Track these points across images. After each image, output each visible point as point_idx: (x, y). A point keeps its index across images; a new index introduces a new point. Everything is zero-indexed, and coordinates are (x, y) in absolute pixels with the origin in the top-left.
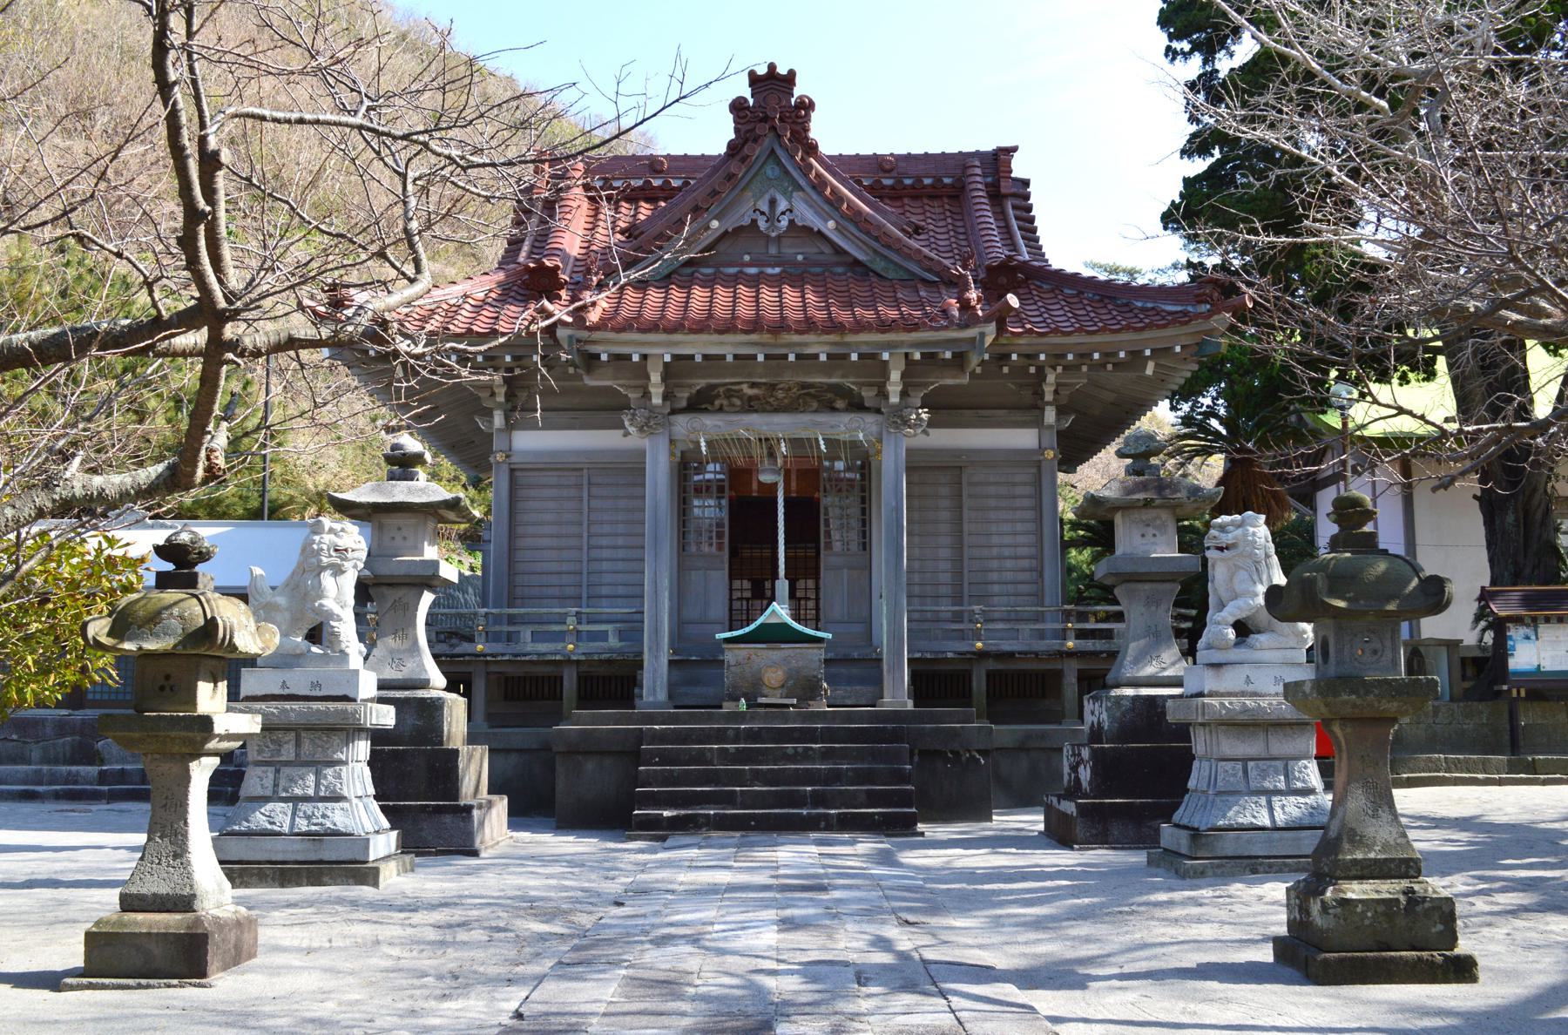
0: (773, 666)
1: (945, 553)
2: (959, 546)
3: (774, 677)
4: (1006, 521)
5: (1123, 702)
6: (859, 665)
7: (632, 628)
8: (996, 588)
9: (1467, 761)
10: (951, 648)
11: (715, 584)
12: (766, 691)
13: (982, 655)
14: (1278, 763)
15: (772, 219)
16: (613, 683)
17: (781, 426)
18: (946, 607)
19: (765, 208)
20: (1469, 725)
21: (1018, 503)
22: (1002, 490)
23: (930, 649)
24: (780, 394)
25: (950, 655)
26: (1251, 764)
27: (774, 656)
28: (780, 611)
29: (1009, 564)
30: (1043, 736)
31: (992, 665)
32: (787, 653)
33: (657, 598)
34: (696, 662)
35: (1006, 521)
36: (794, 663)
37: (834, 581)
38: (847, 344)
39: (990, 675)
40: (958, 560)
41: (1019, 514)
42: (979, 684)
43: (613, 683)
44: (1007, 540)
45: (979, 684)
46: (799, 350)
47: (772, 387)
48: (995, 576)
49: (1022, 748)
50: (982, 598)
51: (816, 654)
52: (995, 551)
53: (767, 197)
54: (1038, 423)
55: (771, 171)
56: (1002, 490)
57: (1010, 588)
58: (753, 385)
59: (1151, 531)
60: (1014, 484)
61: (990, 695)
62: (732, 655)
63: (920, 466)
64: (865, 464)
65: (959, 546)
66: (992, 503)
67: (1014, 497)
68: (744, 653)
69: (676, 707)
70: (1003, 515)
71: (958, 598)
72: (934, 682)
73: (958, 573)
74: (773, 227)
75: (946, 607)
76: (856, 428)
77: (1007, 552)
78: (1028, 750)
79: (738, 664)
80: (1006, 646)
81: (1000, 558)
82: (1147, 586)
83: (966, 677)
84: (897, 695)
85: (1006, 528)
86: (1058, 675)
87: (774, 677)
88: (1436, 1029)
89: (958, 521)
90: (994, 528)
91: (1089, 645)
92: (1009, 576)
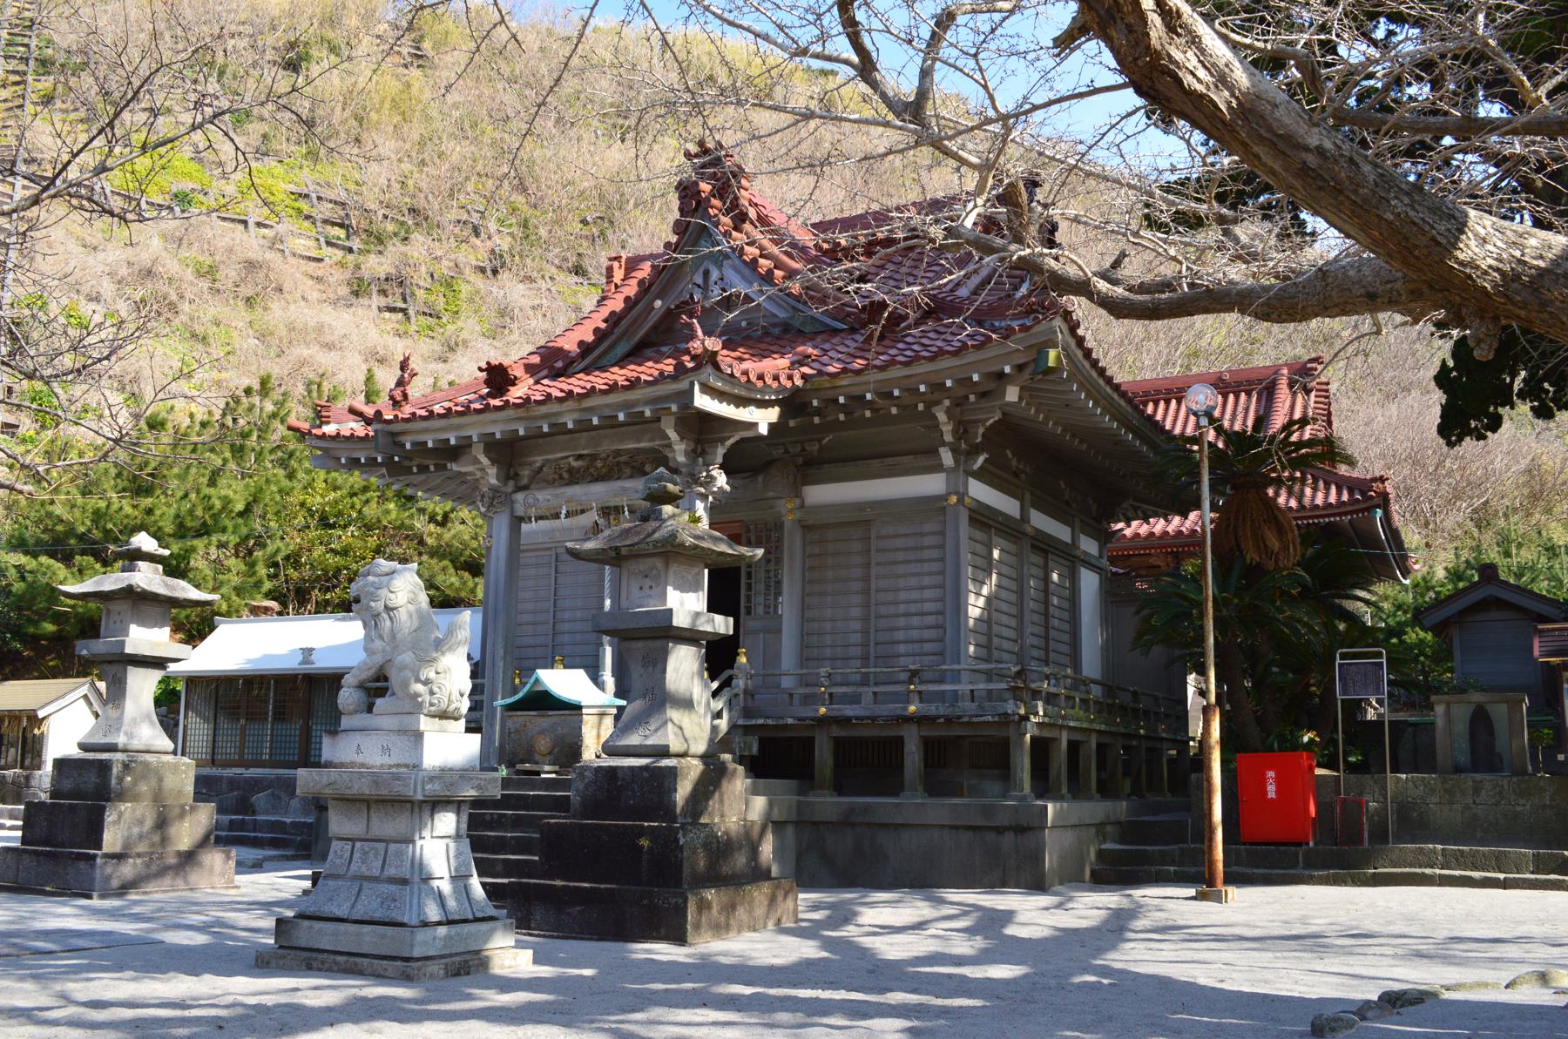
1: (856, 612)
4: (914, 575)
5: (587, 774)
8: (902, 648)
9: (1473, 854)
12: (537, 758)
13: (823, 721)
14: (377, 845)
19: (700, 281)
20: (1524, 807)
21: (926, 554)
22: (911, 542)
24: (599, 464)
25: (790, 721)
26: (358, 844)
29: (915, 621)
30: (867, 809)
31: (836, 731)
32: (554, 719)
35: (914, 575)
36: (560, 731)
38: (536, 418)
39: (838, 743)
41: (926, 567)
42: (823, 754)
44: (915, 595)
45: (823, 754)
46: (553, 420)
47: (593, 457)
48: (901, 635)
49: (846, 822)
52: (902, 608)
53: (701, 270)
54: (938, 468)
56: (911, 542)
57: (916, 647)
58: (580, 457)
59: (648, 582)
60: (922, 535)
61: (838, 765)
66: (900, 556)
67: (923, 548)
68: (521, 720)
70: (911, 568)
71: (865, 659)
74: (706, 297)
77: (913, 608)
78: (853, 825)
79: (517, 731)
80: (849, 711)
81: (907, 615)
82: (640, 644)
85: (913, 582)
86: (899, 742)
90: (902, 583)
91: (932, 709)
92: (915, 634)
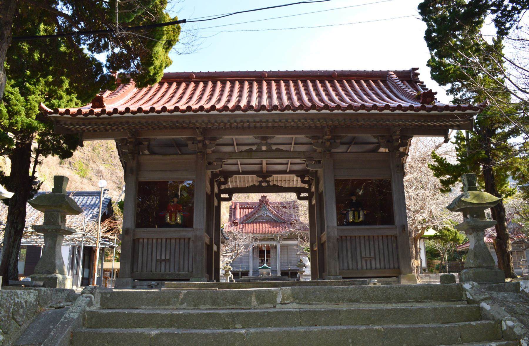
0: (265, 271)
2: (288, 256)
3: (265, 273)
6: (275, 271)
7: (248, 267)
10: (286, 269)
11: (258, 261)
15: (264, 214)
16: (246, 273)
17: (265, 243)
18: (286, 264)
23: (283, 269)
27: (265, 270)
28: (265, 265)
33: (251, 265)
34: (255, 271)
37: (272, 260)
39: (291, 273)
40: (288, 258)
42: (289, 273)
43: (246, 273)
45: (289, 273)
50: (291, 263)
51: (270, 270)
55: (264, 208)
62: (260, 270)
63: (282, 246)
64: (276, 246)
65: (288, 256)
69: (344, 278)
72: (284, 273)
73: (288, 260)
75: (286, 264)
76: (274, 243)
83: (288, 273)
84: (279, 274)
87: (265, 273)
88: (28, 171)
89: (288, 253)
